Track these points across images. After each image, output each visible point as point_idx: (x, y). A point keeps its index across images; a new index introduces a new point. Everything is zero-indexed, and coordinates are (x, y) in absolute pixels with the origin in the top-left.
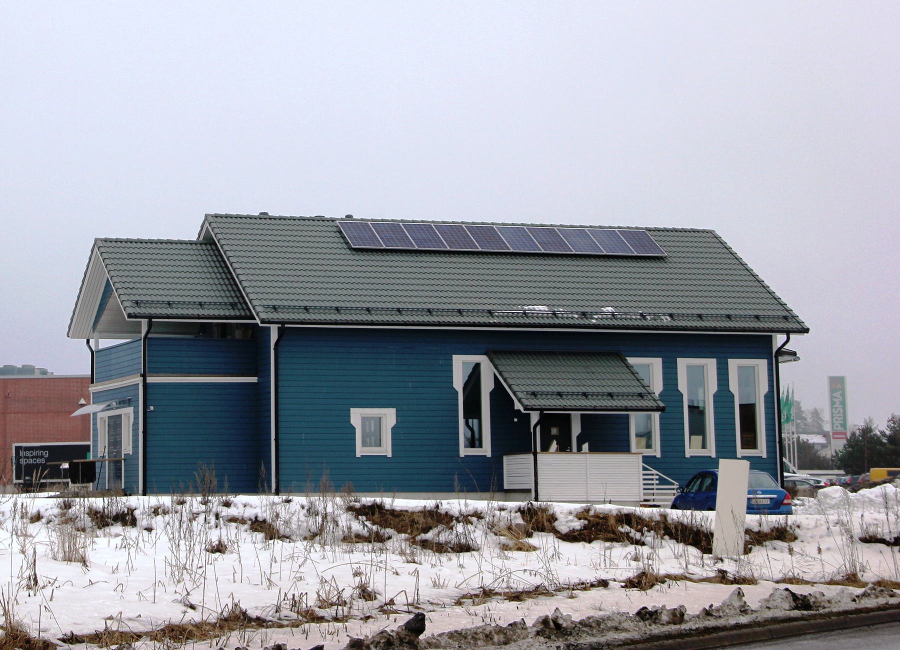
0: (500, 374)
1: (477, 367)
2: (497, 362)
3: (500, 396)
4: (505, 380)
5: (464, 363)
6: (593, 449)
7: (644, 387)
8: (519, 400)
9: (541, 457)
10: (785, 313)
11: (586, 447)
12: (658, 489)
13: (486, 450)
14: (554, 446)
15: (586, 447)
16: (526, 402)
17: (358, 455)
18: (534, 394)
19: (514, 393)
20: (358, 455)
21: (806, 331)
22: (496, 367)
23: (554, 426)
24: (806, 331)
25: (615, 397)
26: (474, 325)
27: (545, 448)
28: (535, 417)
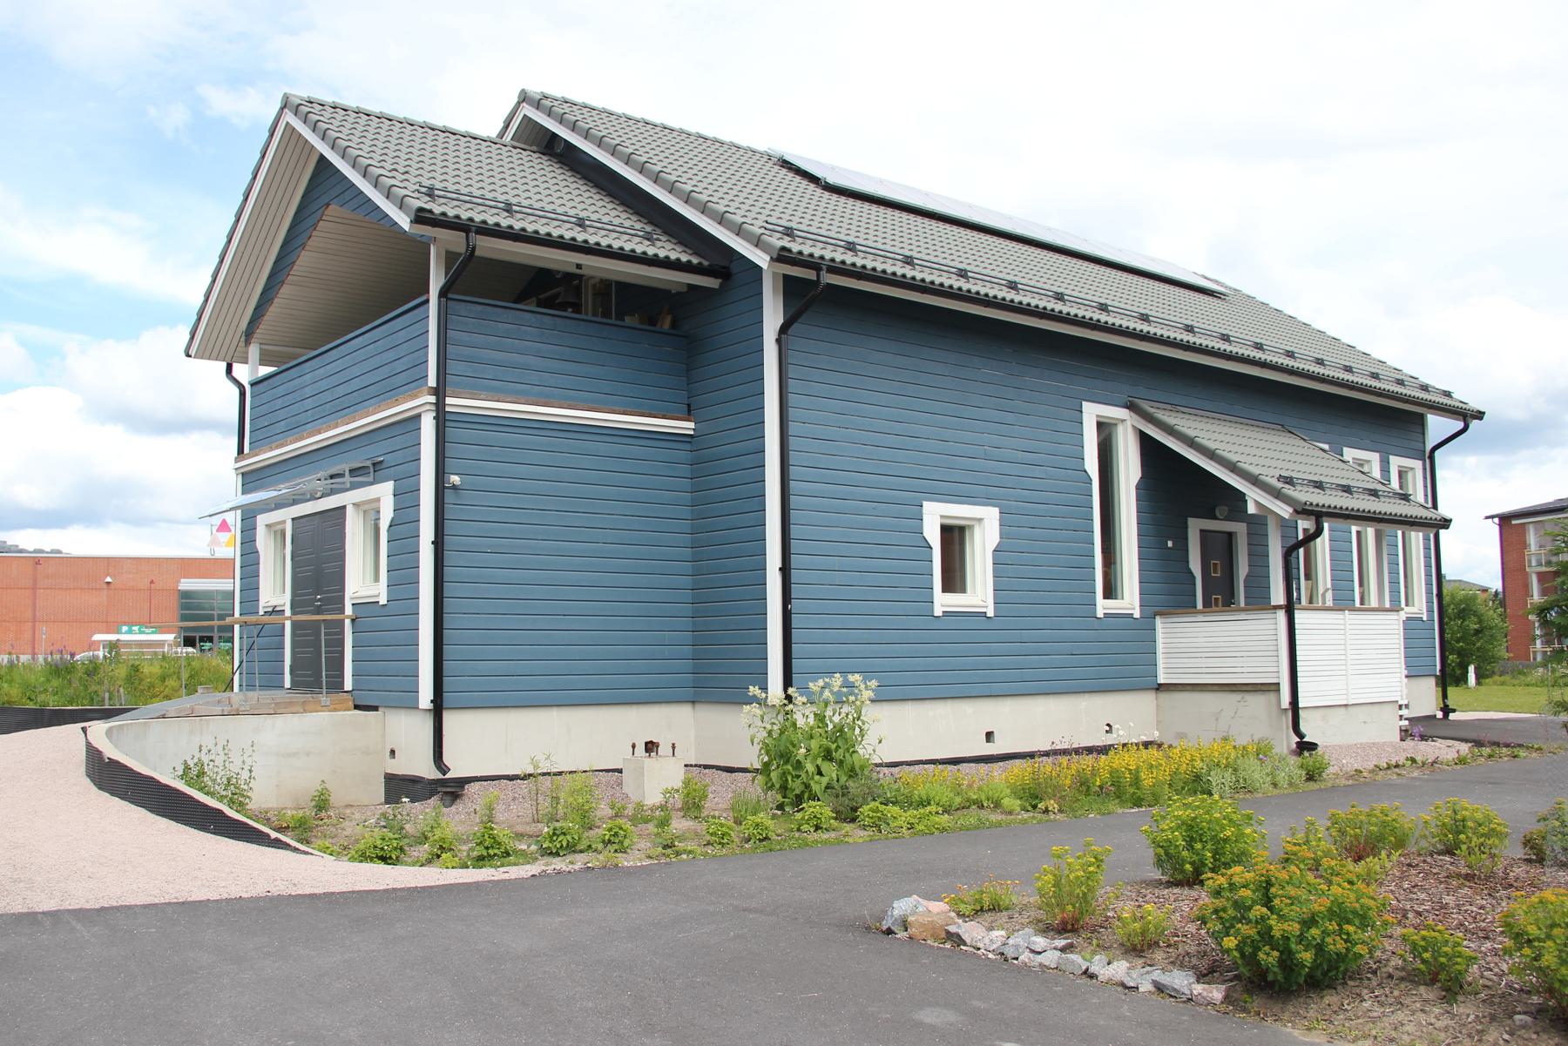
13: (1130, 599)
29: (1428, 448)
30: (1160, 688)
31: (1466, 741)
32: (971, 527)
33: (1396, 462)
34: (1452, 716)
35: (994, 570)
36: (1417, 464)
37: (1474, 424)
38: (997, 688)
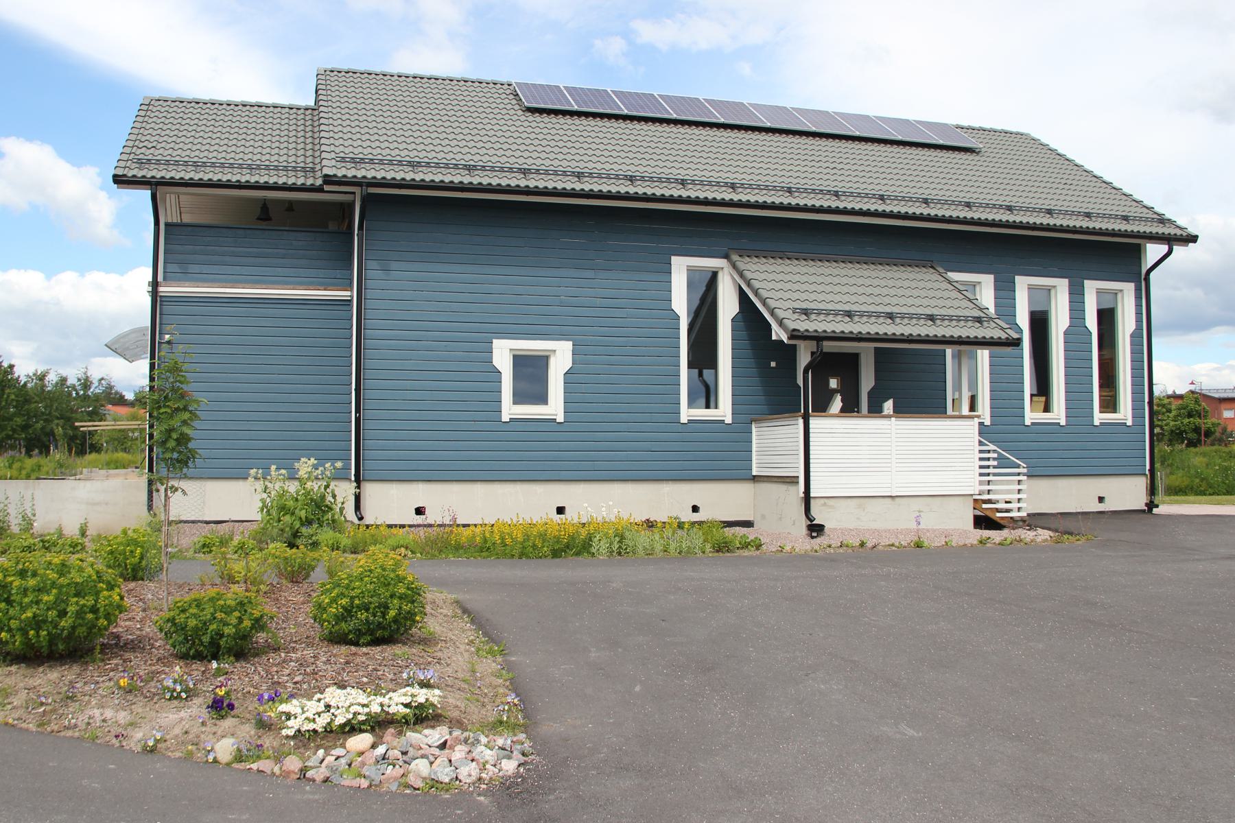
0: (749, 285)
1: (714, 276)
2: (741, 265)
3: (751, 319)
4: (756, 294)
5: (691, 271)
6: (901, 410)
7: (981, 309)
8: (781, 323)
9: (815, 423)
10: (977, 313)
11: (888, 406)
12: (995, 475)
13: (724, 410)
14: (837, 404)
15: (888, 406)
16: (792, 325)
17: (505, 417)
18: (806, 312)
19: (772, 313)
20: (505, 417)
21: (1193, 239)
22: (741, 275)
23: (834, 376)
24: (1193, 239)
25: (938, 322)
26: (706, 202)
27: (821, 407)
28: (804, 359)
29: (1144, 271)
30: (755, 479)
31: (1049, 529)
32: (547, 358)
33: (1022, 284)
34: (1155, 511)
35: (565, 388)
36: (1128, 289)
37: (1178, 250)
38: (564, 475)
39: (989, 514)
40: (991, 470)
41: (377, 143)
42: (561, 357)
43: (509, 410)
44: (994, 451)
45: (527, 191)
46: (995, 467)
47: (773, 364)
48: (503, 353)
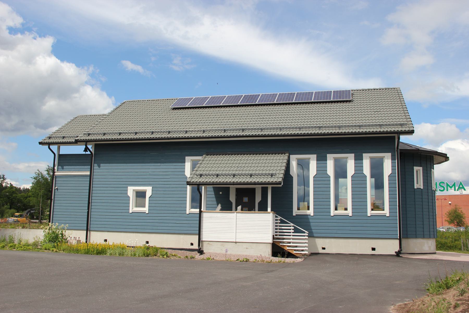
15: (239, 208)
23: (246, 196)
39: (290, 251)
40: (292, 234)
41: (389, 110)
42: (149, 190)
43: (133, 208)
44: (293, 226)
45: (153, 139)
46: (293, 233)
47: (221, 193)
48: (131, 191)
